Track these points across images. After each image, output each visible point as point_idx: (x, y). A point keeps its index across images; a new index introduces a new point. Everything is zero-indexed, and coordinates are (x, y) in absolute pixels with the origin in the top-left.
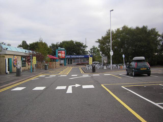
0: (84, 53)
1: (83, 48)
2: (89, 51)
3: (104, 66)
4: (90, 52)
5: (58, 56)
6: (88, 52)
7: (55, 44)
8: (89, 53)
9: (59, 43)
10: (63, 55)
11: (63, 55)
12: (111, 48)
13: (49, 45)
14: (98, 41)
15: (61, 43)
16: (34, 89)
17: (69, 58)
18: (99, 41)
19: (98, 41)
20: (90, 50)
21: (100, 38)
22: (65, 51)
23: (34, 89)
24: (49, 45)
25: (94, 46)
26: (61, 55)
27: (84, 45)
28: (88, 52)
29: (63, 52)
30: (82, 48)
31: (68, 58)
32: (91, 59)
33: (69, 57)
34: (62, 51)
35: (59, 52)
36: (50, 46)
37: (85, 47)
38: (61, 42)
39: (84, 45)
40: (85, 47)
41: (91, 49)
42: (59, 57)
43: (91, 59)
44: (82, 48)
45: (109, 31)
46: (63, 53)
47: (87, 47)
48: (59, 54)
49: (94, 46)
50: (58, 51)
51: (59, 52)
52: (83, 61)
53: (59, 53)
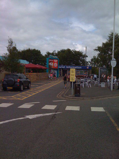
0: (84, 62)
1: (83, 58)
2: (89, 62)
3: (102, 83)
4: (90, 63)
5: (49, 65)
6: (89, 63)
7: (51, 52)
8: (89, 64)
9: (56, 52)
10: (56, 65)
11: (56, 65)
12: (113, 56)
13: (44, 53)
14: (97, 48)
15: (59, 52)
16: (19, 107)
17: (64, 68)
18: (99, 49)
19: (97, 48)
20: (90, 61)
21: (101, 45)
22: (58, 61)
23: (19, 107)
24: (44, 53)
25: (94, 56)
26: (52, 64)
27: (83, 54)
28: (89, 63)
29: (56, 61)
30: (81, 58)
31: (63, 69)
32: (73, 72)
33: (63, 67)
34: (54, 60)
35: (50, 60)
36: (46, 55)
37: (85, 56)
38: (59, 50)
39: (83, 54)
40: (85, 56)
41: (92, 60)
42: (50, 66)
43: (73, 72)
44: (81, 58)
45: (112, 35)
46: (56, 62)
47: (87, 57)
48: (50, 64)
49: (94, 56)
50: (50, 59)
51: (50, 60)
52: (79, 73)
53: (50, 62)
